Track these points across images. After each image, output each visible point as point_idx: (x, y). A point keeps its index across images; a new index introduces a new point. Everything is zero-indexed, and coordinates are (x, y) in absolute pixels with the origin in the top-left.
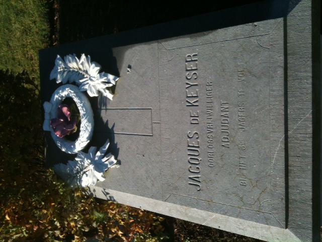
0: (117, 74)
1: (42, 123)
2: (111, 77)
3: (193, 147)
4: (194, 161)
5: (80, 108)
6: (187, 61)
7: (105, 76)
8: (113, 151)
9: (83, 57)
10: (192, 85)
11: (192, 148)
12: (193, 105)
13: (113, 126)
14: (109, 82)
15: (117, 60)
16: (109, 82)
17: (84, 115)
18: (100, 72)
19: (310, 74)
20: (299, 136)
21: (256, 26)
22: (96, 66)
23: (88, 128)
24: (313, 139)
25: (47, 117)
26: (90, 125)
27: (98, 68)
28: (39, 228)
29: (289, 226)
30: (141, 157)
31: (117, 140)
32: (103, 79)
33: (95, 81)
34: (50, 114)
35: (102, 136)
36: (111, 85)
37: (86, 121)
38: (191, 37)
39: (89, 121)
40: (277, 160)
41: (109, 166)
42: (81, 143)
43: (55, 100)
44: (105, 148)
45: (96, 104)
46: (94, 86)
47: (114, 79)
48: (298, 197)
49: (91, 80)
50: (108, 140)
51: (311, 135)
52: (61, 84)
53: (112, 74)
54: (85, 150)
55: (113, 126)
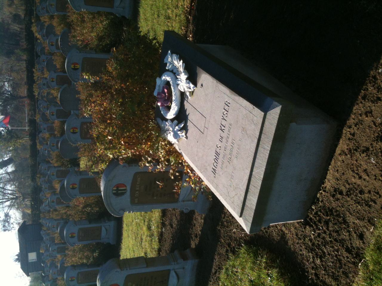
0: (195, 84)
1: (153, 92)
2: (192, 86)
3: (217, 153)
4: (216, 159)
5: (173, 94)
6: (225, 104)
7: (189, 83)
8: (185, 129)
9: (181, 61)
10: (224, 119)
11: (217, 154)
12: (222, 131)
13: (189, 114)
14: (190, 88)
15: (198, 73)
16: (190, 88)
17: (174, 100)
18: (187, 79)
19: (269, 149)
20: (257, 177)
21: (254, 108)
22: (185, 75)
23: (175, 109)
24: (129, 259)
25: (157, 88)
26: (177, 107)
27: (186, 76)
28: (160, 49)
29: (242, 217)
30: (196, 142)
31: (189, 124)
32: (188, 85)
33: (183, 83)
34: (159, 86)
35: (182, 117)
36: (190, 90)
37: (175, 104)
38: (230, 91)
39: (176, 105)
40: (244, 183)
41: (181, 137)
42: (171, 115)
43: (163, 79)
44: (181, 125)
45: (183, 95)
46: (182, 86)
47: (193, 88)
48: (249, 206)
49: (181, 81)
50: (184, 121)
51: (262, 179)
52: (168, 70)
53: (193, 84)
54: (172, 120)
55: (189, 114)
